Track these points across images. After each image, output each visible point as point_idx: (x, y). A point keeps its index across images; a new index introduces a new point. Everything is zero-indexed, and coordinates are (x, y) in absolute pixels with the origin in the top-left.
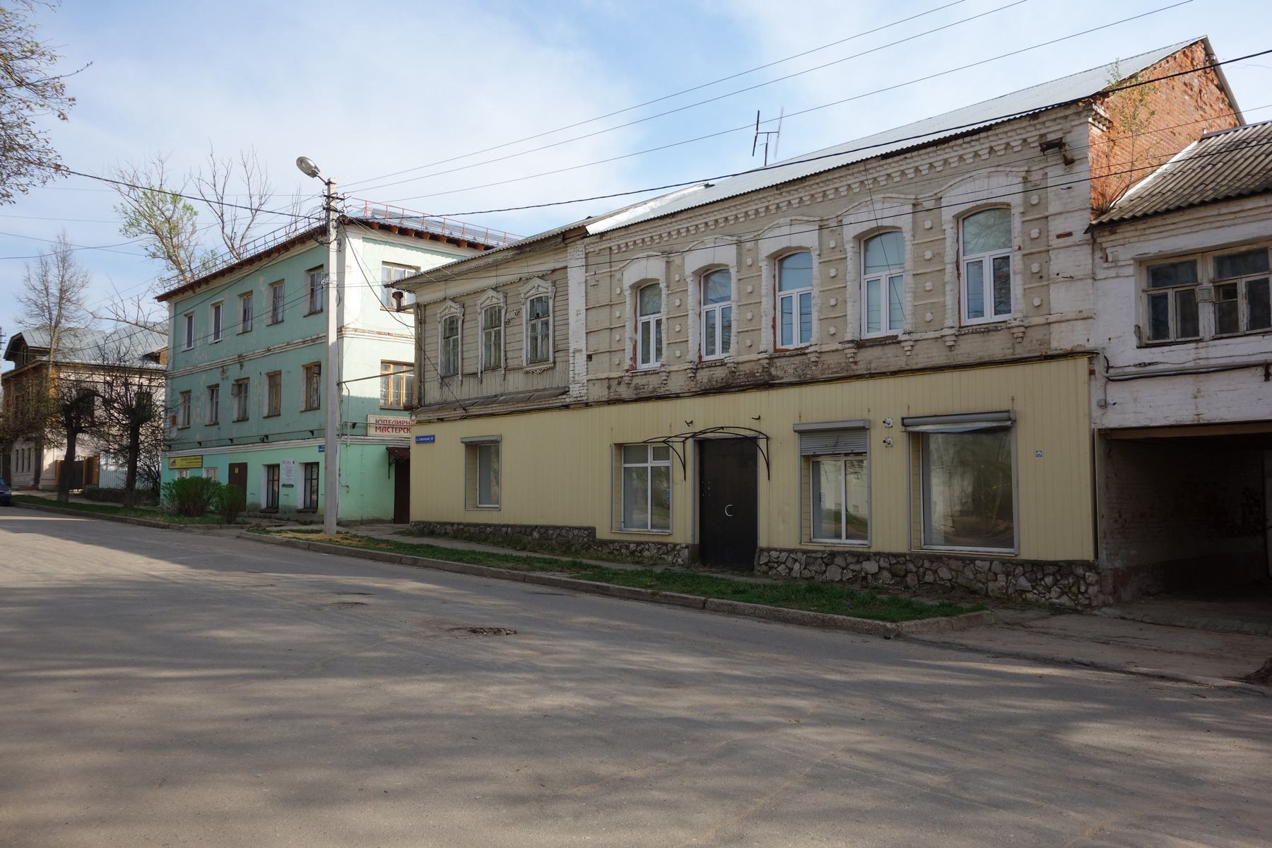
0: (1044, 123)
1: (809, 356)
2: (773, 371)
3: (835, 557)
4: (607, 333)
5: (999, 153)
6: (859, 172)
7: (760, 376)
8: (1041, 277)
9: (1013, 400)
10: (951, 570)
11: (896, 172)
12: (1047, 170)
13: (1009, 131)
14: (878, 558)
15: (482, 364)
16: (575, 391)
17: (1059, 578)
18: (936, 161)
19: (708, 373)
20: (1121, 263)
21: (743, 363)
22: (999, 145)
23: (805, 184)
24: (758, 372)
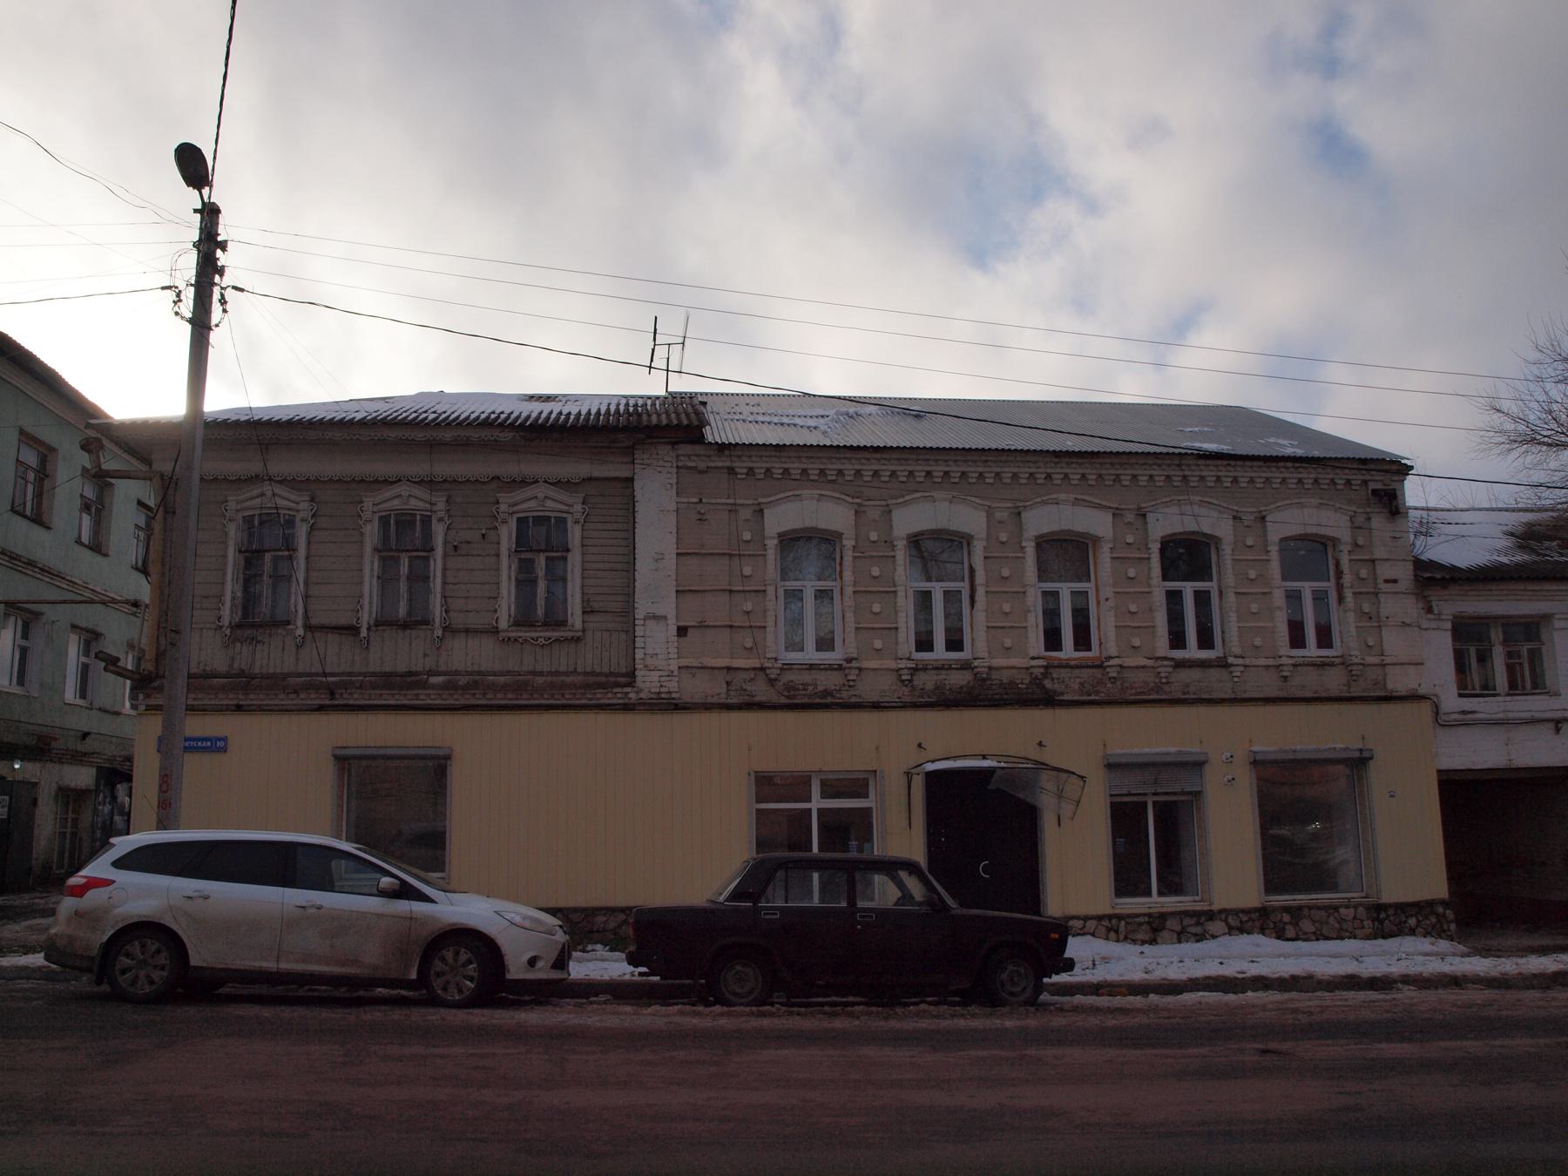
0: (750, 456)
1: (1108, 670)
2: (1048, 684)
3: (1166, 920)
5: (936, 480)
7: (1027, 688)
8: (1370, 618)
10: (1314, 922)
11: (1212, 476)
14: (1223, 916)
16: (649, 682)
17: (1421, 918)
18: (1243, 477)
19: (935, 677)
20: (1443, 617)
24: (1022, 683)
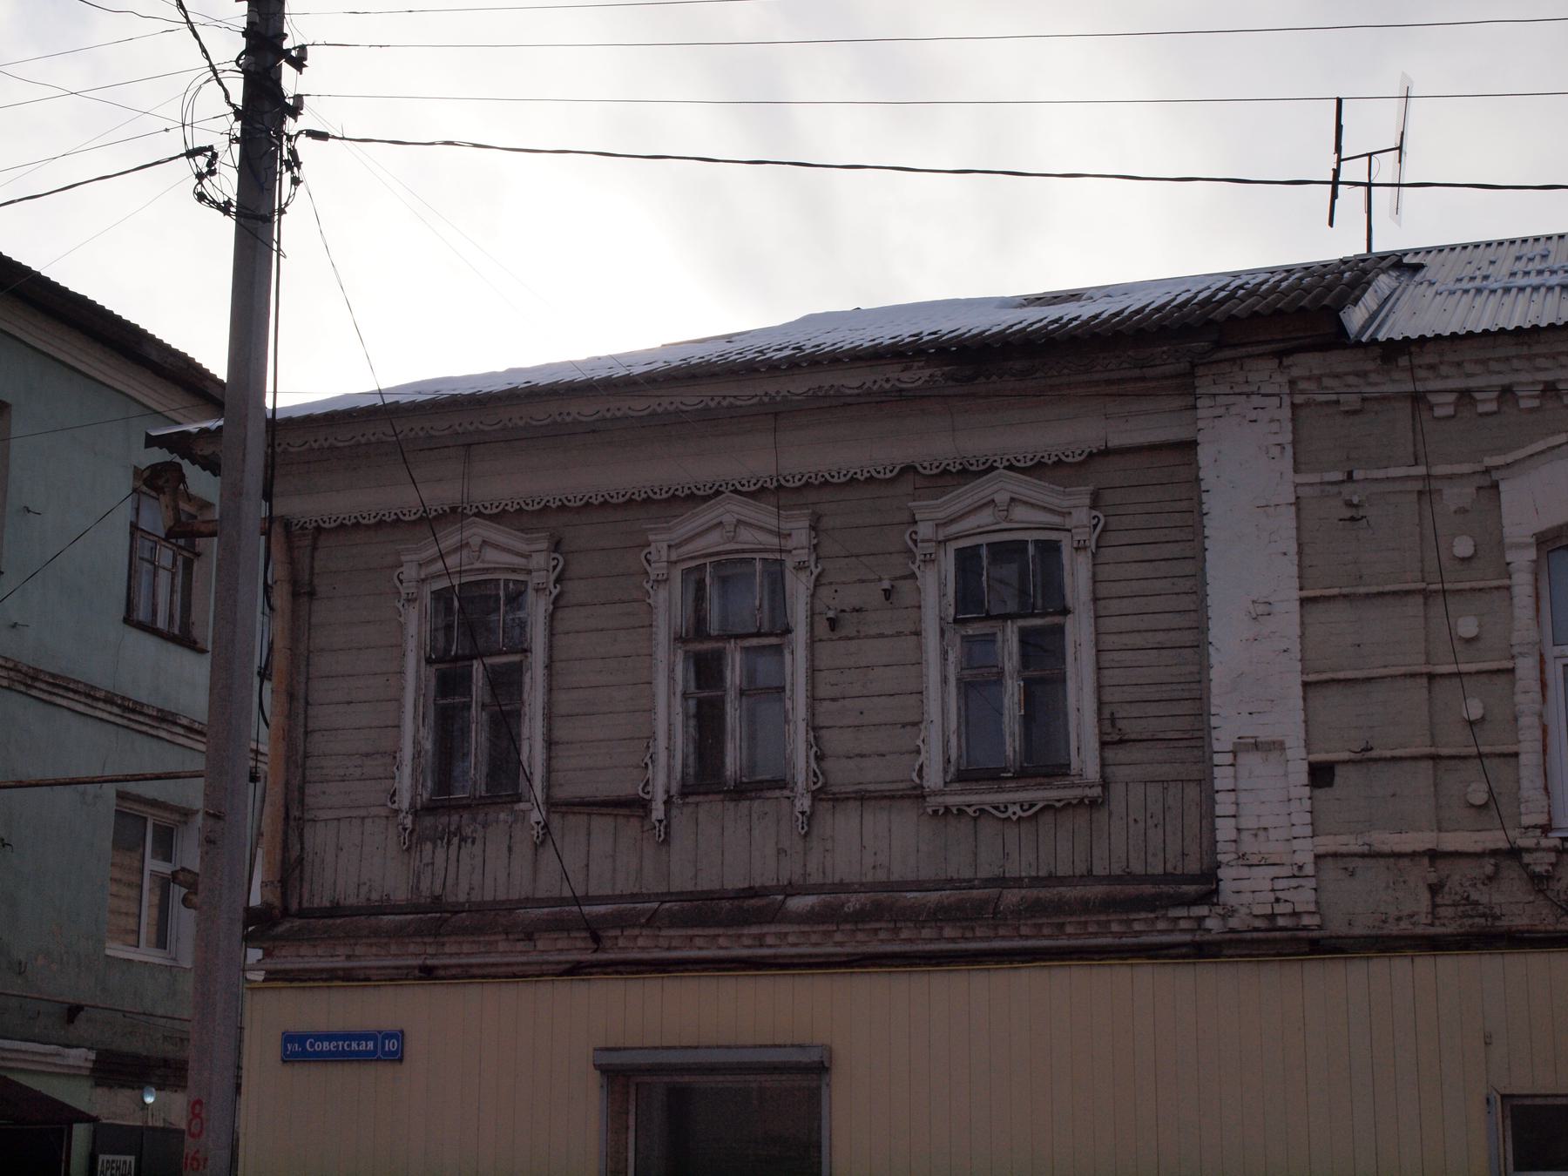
4: (1418, 690)
15: (670, 768)
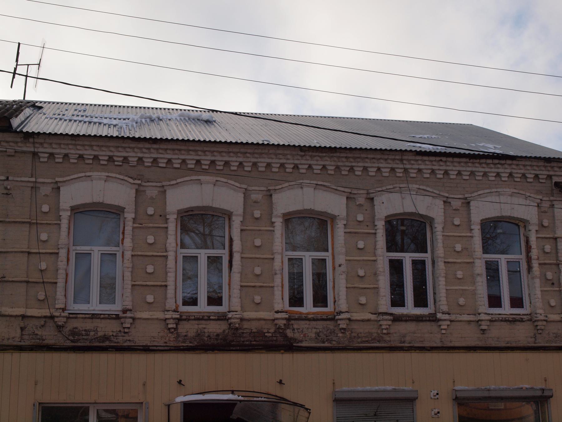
1: (339, 322)
2: (289, 333)
6: (394, 160)
7: (272, 336)
9: (546, 381)
12: (555, 203)
13: (412, 160)
19: (196, 326)
21: (249, 320)
22: (206, 159)
23: (335, 155)
24: (268, 332)
